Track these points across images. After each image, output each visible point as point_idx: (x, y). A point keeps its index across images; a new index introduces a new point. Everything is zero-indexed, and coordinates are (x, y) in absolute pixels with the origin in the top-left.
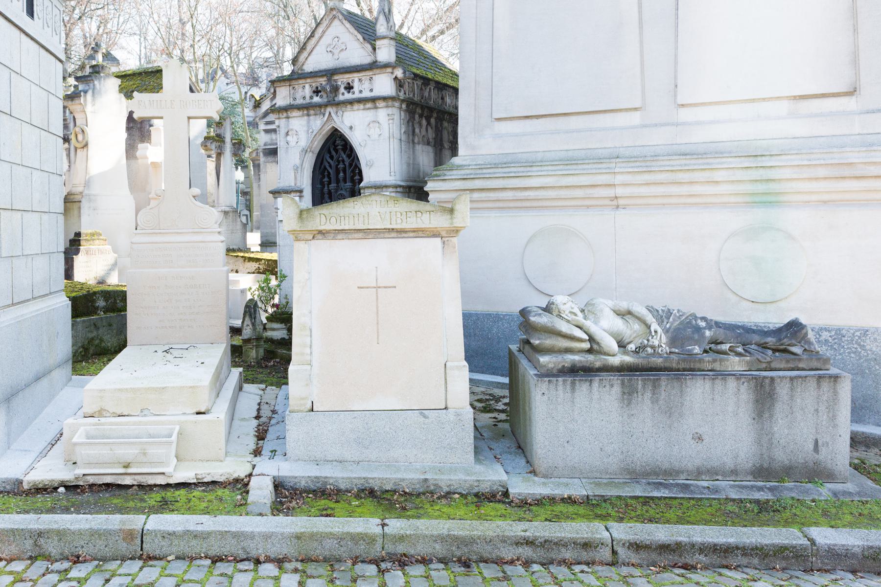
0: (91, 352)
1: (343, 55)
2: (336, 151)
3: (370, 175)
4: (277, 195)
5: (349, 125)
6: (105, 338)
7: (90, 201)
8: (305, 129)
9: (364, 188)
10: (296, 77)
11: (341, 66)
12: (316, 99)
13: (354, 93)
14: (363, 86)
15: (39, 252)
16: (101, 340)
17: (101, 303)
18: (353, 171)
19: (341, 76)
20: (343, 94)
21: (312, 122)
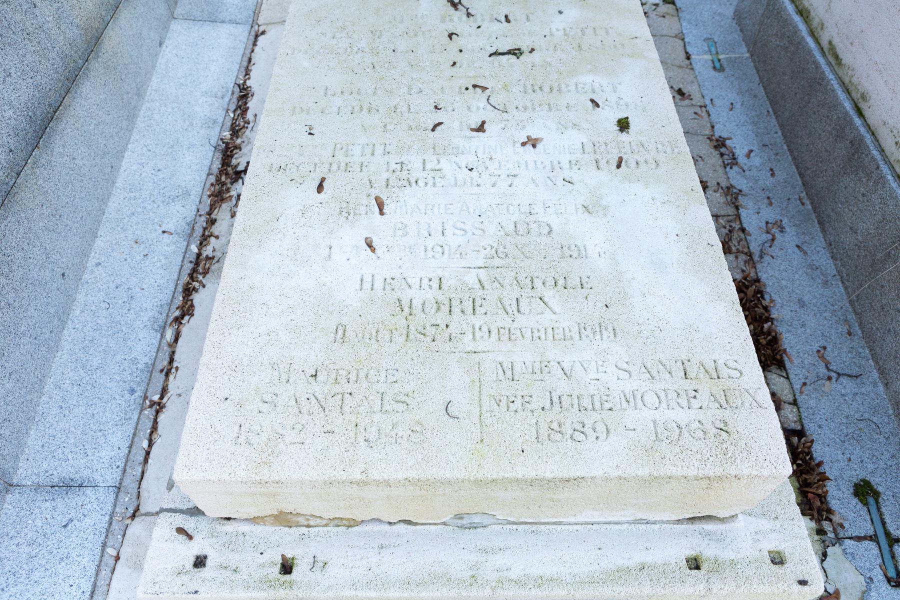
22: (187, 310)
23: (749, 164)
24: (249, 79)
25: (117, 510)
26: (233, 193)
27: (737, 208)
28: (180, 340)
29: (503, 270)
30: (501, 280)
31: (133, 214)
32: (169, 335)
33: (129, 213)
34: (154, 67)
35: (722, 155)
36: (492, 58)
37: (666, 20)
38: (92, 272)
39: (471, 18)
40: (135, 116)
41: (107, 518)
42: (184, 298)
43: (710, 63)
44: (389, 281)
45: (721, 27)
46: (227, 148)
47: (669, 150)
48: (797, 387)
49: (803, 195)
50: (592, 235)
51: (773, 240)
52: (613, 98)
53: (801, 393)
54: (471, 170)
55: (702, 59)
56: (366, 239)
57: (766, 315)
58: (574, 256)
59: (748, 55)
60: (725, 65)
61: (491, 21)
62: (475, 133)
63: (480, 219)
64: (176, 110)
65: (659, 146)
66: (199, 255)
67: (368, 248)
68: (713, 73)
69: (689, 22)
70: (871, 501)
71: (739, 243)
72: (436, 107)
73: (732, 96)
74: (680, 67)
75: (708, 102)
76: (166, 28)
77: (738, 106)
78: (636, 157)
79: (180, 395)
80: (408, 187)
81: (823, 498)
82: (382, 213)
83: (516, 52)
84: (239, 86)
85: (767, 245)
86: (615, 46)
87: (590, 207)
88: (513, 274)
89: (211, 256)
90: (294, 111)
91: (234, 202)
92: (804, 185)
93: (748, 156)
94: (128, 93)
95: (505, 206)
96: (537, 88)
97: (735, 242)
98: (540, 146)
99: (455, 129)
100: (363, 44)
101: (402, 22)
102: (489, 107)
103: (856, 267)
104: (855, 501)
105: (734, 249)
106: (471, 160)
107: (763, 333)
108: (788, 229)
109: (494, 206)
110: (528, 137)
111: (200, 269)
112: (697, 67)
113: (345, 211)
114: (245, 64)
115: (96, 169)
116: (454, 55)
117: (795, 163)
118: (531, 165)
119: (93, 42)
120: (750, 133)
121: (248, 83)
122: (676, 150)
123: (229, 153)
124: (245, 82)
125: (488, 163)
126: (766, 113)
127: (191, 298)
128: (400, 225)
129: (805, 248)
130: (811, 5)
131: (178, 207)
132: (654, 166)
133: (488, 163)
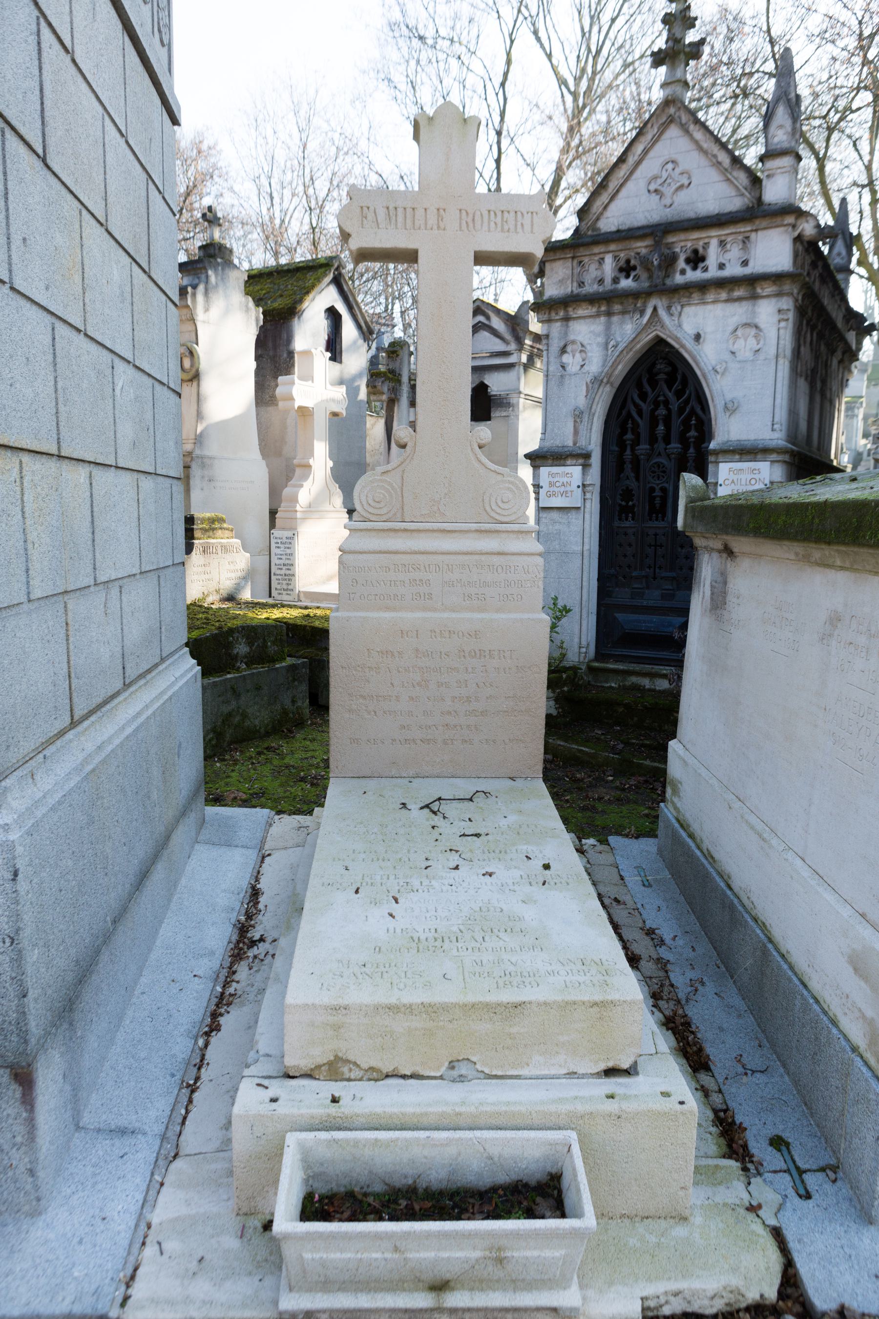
0: (228, 738)
1: (682, 198)
2: (653, 383)
3: (727, 429)
4: (538, 462)
5: (694, 332)
7: (203, 466)
8: (601, 340)
9: (716, 453)
10: (584, 242)
11: (676, 218)
12: (626, 283)
13: (706, 269)
14: (723, 257)
15: (135, 570)
16: (244, 716)
17: (242, 649)
18: (686, 424)
19: (682, 236)
20: (683, 272)
21: (615, 328)
25: (162, 1151)
27: (666, 972)
28: (209, 1048)
32: (201, 1042)
35: (653, 939)
38: (138, 998)
41: (155, 1155)
48: (721, 1080)
50: (529, 913)
51: (696, 990)
52: (540, 856)
53: (724, 1084)
55: (633, 880)
60: (652, 883)
66: (222, 994)
68: (643, 888)
69: (622, 856)
70: (784, 1148)
75: (639, 906)
77: (664, 908)
79: (211, 1080)
81: (745, 1147)
83: (478, 835)
100: (375, 830)
104: (770, 1148)
105: (665, 997)
106: (452, 882)
108: (708, 984)
112: (630, 885)
114: (255, 874)
116: (437, 836)
131: (206, 960)
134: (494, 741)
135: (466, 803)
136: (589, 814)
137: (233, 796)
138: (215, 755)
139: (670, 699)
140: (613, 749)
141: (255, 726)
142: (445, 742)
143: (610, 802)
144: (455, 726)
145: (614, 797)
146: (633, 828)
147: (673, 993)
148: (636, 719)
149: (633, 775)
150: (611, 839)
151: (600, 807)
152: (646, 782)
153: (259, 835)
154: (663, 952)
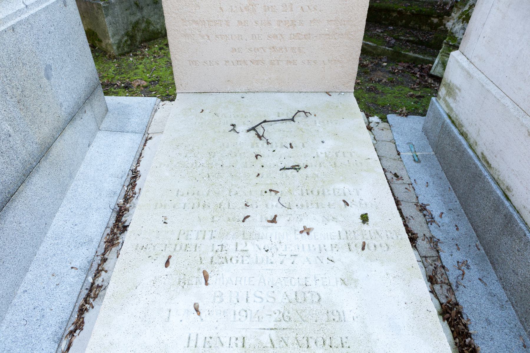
0: (139, 38)
6: (152, 19)
16: (149, 23)
22: (79, 325)
23: (442, 222)
24: (139, 166)
26: (120, 240)
27: (438, 251)
29: (287, 331)
30: (286, 339)
31: (54, 255)
33: (51, 254)
34: (83, 159)
35: (425, 215)
36: (282, 171)
37: (384, 132)
38: (20, 296)
39: (269, 145)
40: (66, 190)
42: (78, 316)
43: (412, 158)
44: (208, 340)
45: (416, 136)
46: (120, 210)
47: (395, 237)
49: (478, 243)
51: (463, 274)
54: (267, 251)
55: (406, 155)
56: (195, 304)
57: (466, 331)
58: (336, 320)
59: (433, 153)
60: (420, 158)
61: (282, 147)
62: (270, 224)
63: (273, 289)
64: (92, 185)
65: (388, 234)
66: (93, 284)
67: (195, 312)
68: (414, 163)
69: (398, 133)
71: (442, 276)
72: (246, 205)
73: (427, 178)
74: (395, 160)
75: (413, 182)
76: (94, 136)
77: (431, 184)
78: (374, 242)
80: (225, 264)
82: (206, 284)
83: (296, 168)
84: (132, 171)
85: (460, 278)
86: (357, 164)
87: (346, 280)
88: (294, 335)
89: (100, 285)
90: (156, 206)
91: (120, 246)
92: (478, 236)
93: (441, 216)
94: (64, 177)
95: (289, 279)
96: (309, 192)
97: (439, 276)
98: (311, 233)
99: (258, 223)
100: (203, 161)
101: (228, 147)
102: (279, 205)
103: (521, 298)
105: (439, 280)
107: (466, 346)
108: (472, 267)
109: (282, 279)
110: (304, 227)
111: (92, 295)
112: (405, 160)
113: (182, 281)
114: (138, 157)
115: (35, 227)
117: (470, 222)
118: (306, 248)
119: (45, 150)
120: (440, 201)
121: (138, 169)
122: (400, 237)
123: (121, 214)
124: (136, 168)
125: (278, 246)
126: (448, 189)
127: (83, 316)
128: (218, 294)
129: (485, 281)
130: (468, 131)
132: (386, 249)
133: (278, 246)
134: (315, 62)
135: (288, 122)
136: (373, 94)
137: (137, 84)
138: (131, 52)
139: (430, 7)
140: (388, 44)
141: (158, 30)
142: (272, 63)
143: (386, 84)
144: (281, 49)
145: (389, 80)
146: (404, 108)
147: (444, 276)
148: (404, 21)
149: (400, 62)
150: (390, 117)
151: (380, 88)
152: (409, 67)
153: (146, 121)
154: (438, 234)
